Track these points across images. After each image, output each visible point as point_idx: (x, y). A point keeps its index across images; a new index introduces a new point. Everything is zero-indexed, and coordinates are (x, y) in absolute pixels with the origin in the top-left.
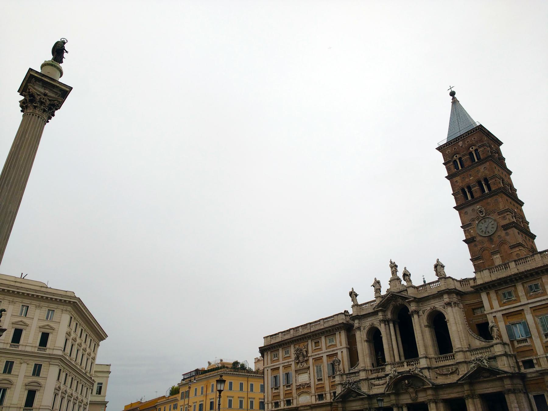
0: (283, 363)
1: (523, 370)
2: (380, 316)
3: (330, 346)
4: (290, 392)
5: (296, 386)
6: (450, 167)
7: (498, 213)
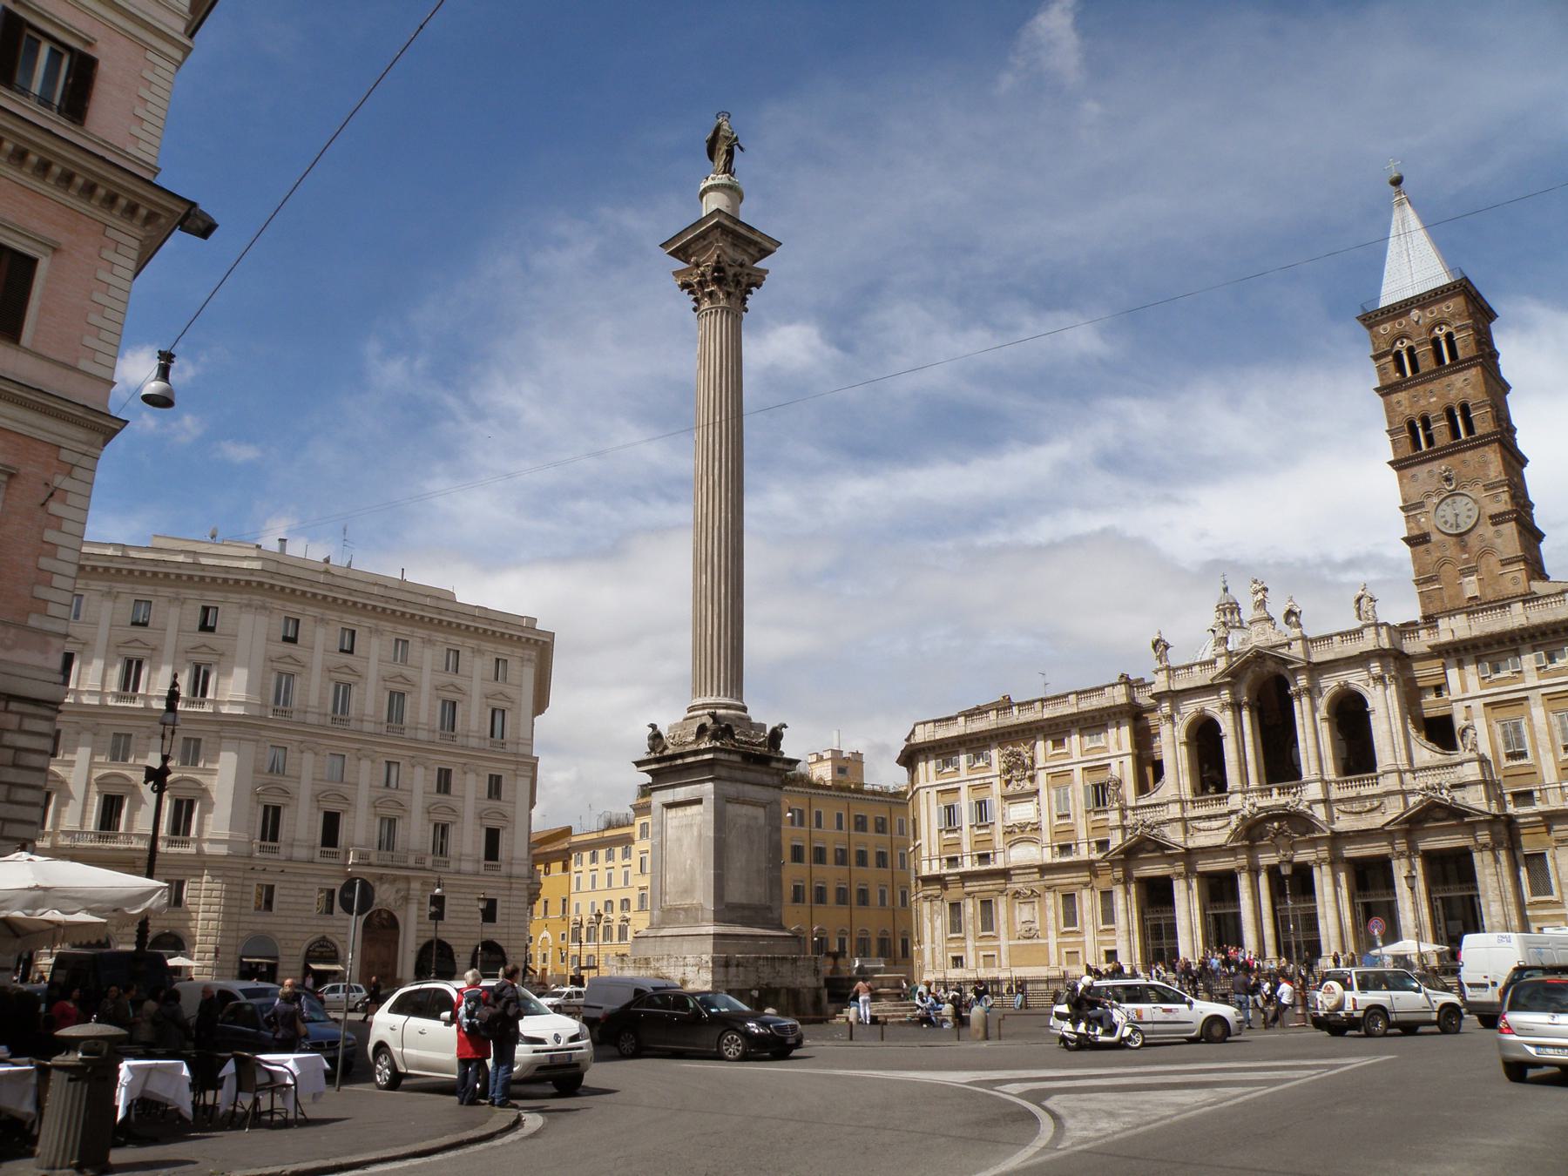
0: (969, 780)
1: (1511, 809)
2: (1226, 695)
4: (989, 838)
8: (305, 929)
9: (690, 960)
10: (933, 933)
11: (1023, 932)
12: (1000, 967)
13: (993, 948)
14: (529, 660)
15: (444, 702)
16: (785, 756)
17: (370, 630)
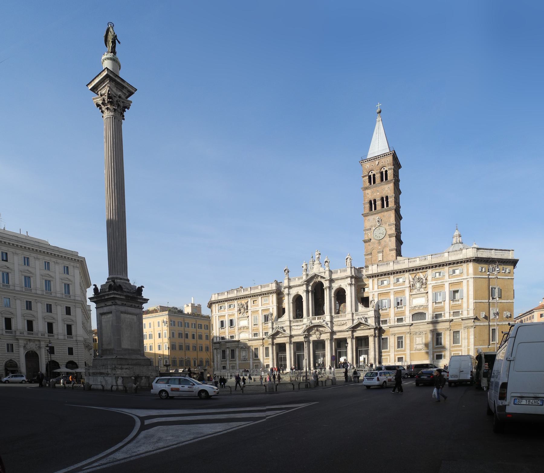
3: (265, 304)
4: (234, 331)
5: (238, 327)
6: (366, 180)
7: (389, 224)
8: (3, 357)
9: (109, 367)
10: (217, 359)
11: (243, 359)
12: (236, 369)
13: (234, 364)
14: (76, 267)
15: (65, 284)
16: (144, 298)
17: (74, 267)
